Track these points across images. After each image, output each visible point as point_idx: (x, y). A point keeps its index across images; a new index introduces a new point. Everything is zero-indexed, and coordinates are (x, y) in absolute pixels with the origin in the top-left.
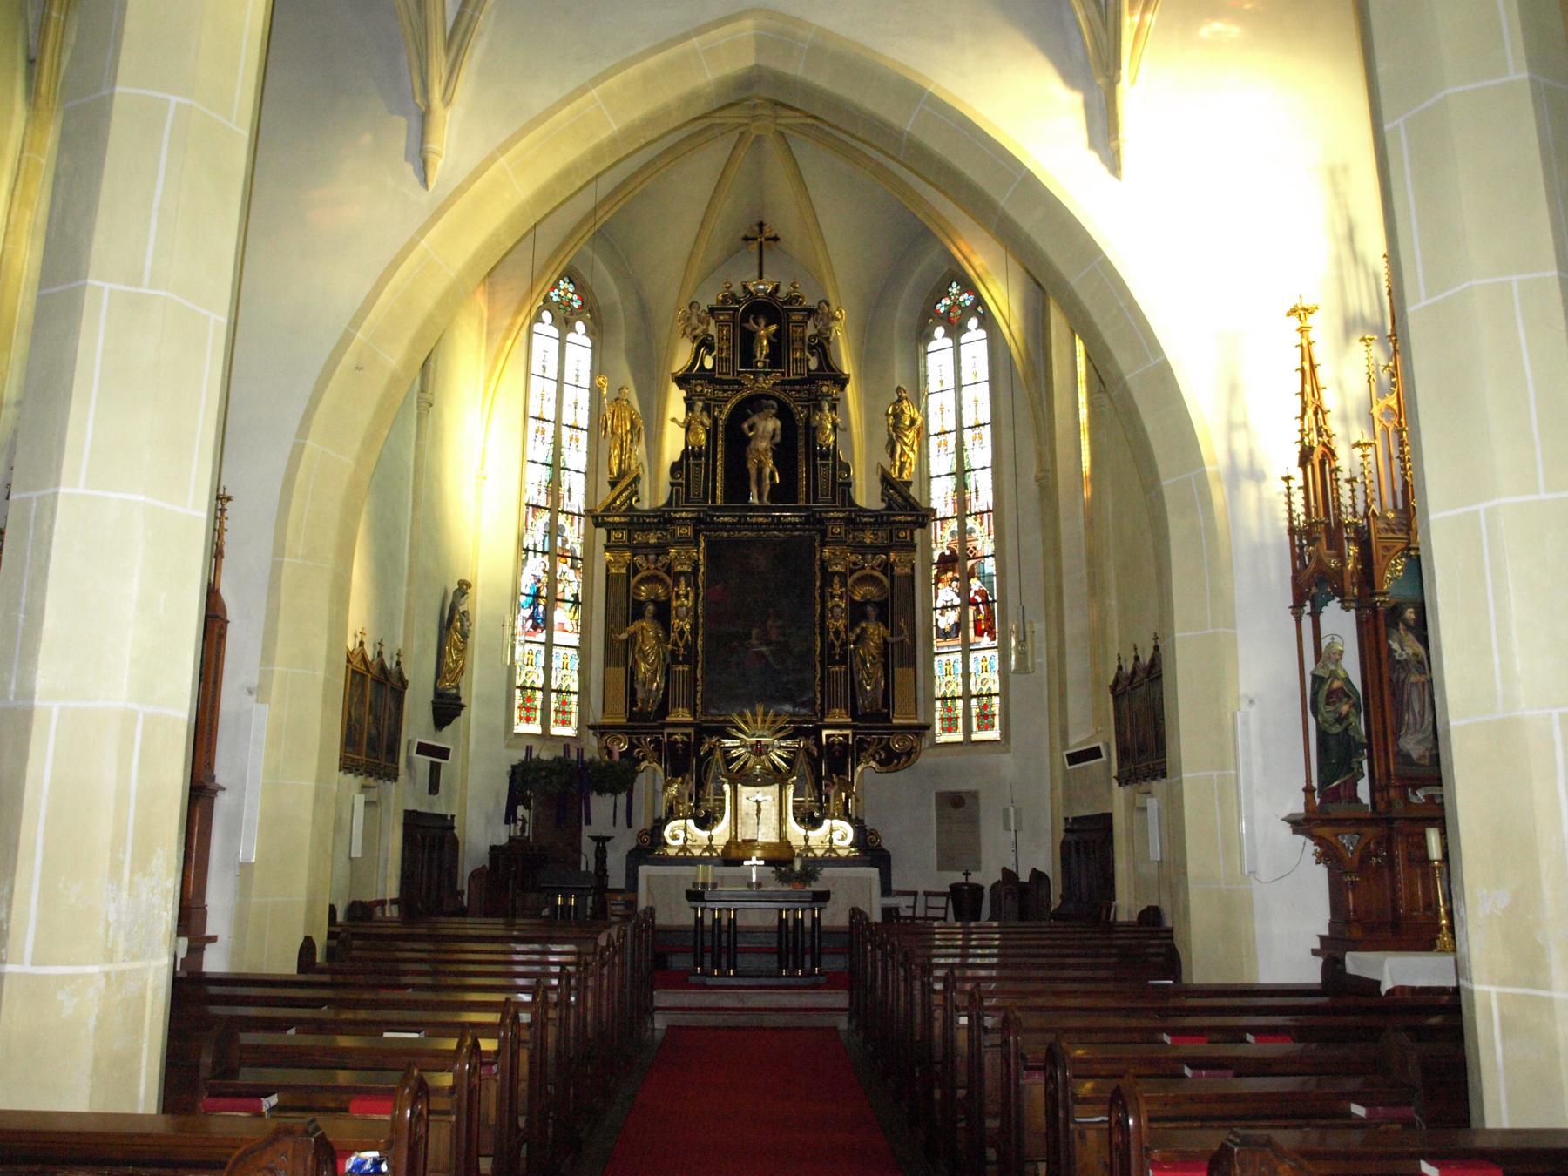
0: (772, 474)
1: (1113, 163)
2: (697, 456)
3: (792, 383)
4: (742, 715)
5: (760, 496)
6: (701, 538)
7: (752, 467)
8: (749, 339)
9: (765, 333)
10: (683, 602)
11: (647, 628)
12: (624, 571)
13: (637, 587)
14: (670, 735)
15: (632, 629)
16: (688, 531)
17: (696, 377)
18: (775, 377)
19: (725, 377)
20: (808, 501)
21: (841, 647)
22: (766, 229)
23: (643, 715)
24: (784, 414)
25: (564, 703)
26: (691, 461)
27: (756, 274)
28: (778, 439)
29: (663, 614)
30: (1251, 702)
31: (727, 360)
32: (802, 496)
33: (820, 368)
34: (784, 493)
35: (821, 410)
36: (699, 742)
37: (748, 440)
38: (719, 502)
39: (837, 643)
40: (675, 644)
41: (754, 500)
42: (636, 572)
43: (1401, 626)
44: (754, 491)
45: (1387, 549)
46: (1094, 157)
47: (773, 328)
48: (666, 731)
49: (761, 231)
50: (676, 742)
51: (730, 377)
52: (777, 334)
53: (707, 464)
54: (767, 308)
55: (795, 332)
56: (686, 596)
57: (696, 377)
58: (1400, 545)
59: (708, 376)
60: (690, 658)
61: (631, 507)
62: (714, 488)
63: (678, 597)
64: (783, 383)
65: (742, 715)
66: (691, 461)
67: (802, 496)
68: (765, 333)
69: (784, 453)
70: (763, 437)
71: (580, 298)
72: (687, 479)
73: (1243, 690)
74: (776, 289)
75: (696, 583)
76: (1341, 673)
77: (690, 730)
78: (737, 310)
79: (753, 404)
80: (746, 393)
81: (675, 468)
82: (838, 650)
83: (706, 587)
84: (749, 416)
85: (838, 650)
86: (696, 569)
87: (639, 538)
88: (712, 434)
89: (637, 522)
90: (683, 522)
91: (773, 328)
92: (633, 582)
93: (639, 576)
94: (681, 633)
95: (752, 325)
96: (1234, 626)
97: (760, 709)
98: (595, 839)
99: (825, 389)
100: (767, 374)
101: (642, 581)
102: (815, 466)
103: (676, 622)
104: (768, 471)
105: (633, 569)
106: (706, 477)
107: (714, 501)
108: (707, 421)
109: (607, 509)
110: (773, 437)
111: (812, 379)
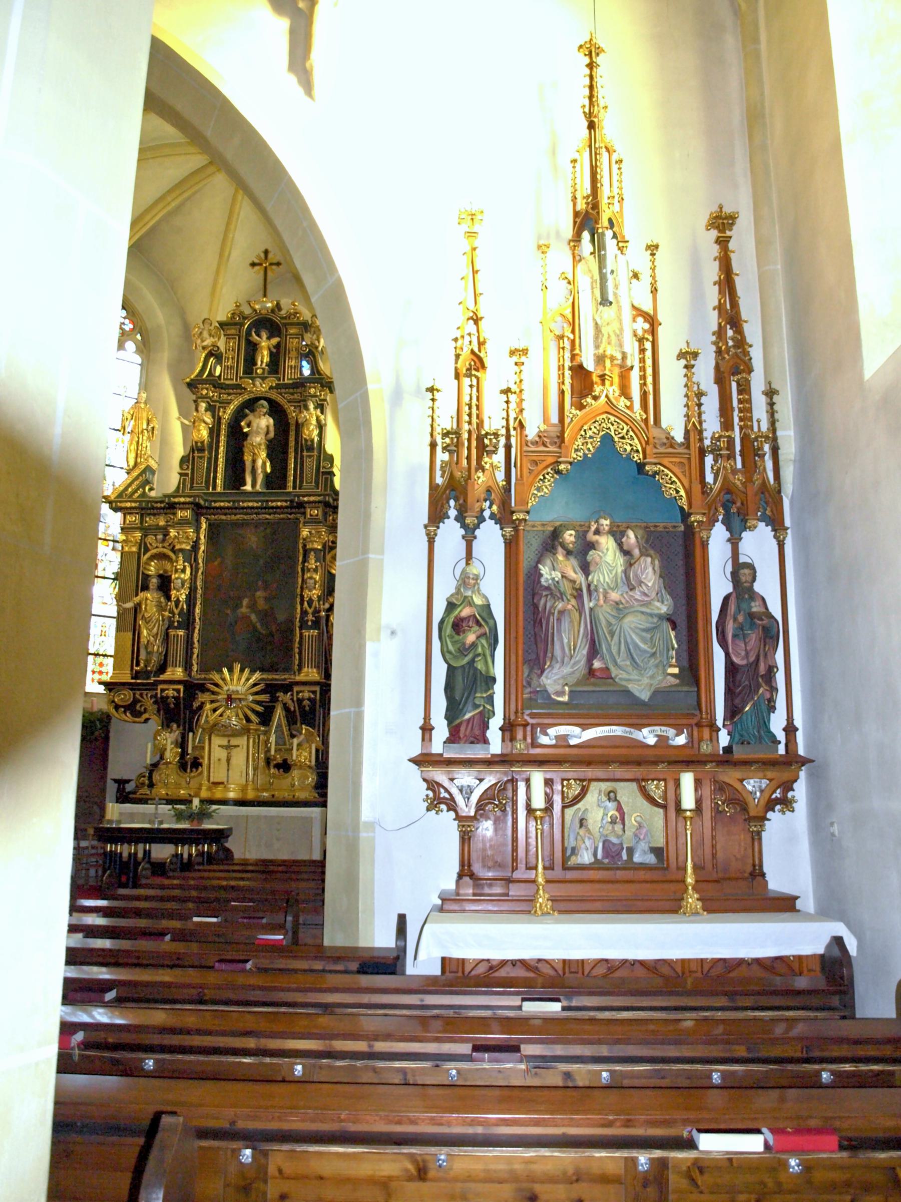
0: (264, 463)
1: (307, 83)
2: (201, 450)
3: (286, 386)
4: (242, 670)
5: (254, 485)
6: (203, 520)
7: (248, 458)
8: (252, 349)
9: (265, 344)
10: (182, 575)
11: (150, 597)
12: (134, 549)
13: (147, 563)
14: (163, 690)
15: (137, 600)
16: (188, 514)
17: (205, 382)
18: (272, 381)
19: (227, 382)
20: (294, 488)
21: (314, 613)
22: (270, 256)
23: (146, 674)
24: (276, 410)
25: (101, 665)
26: (196, 454)
27: (262, 292)
28: (272, 435)
29: (165, 585)
30: (393, 633)
31: (232, 367)
32: (290, 484)
33: (312, 373)
34: (276, 480)
35: (306, 408)
36: (193, 697)
37: (246, 435)
38: (219, 489)
39: (310, 611)
40: (171, 612)
41: (248, 488)
42: (147, 550)
43: (560, 549)
44: (249, 480)
45: (536, 463)
46: (293, 79)
47: (275, 341)
48: (160, 687)
49: (266, 257)
50: (167, 697)
51: (234, 382)
52: (278, 346)
53: (210, 459)
54: (269, 324)
55: (293, 343)
56: (184, 571)
57: (205, 382)
58: (550, 460)
59: (216, 383)
60: (188, 623)
61: (144, 494)
62: (215, 478)
63: (176, 571)
64: (278, 387)
65: (242, 670)
66: (196, 454)
67: (290, 484)
68: (265, 344)
69: (277, 449)
70: (258, 433)
71: (132, 322)
72: (193, 469)
73: (384, 622)
74: (278, 307)
75: (196, 560)
76: (478, 601)
77: (181, 687)
78: (243, 325)
79: (251, 405)
80: (247, 397)
81: (184, 461)
82: (310, 617)
83: (207, 562)
84: (246, 415)
85: (310, 617)
86: (195, 546)
87: (150, 521)
88: (214, 432)
89: (147, 508)
90: (183, 506)
91: (275, 341)
92: (144, 558)
93: (148, 555)
94: (178, 602)
95: (255, 338)
96: (382, 553)
97: (237, 667)
98: (115, 781)
99: (312, 391)
100: (263, 379)
101: (152, 558)
102: (302, 457)
103: (173, 593)
104: (259, 463)
105: (144, 547)
106: (209, 469)
107: (214, 488)
108: (208, 418)
109: (120, 495)
110: (267, 433)
111: (300, 384)
